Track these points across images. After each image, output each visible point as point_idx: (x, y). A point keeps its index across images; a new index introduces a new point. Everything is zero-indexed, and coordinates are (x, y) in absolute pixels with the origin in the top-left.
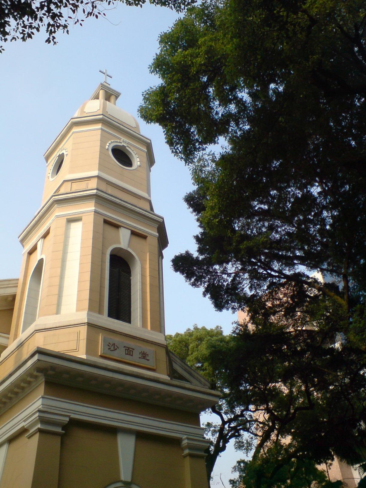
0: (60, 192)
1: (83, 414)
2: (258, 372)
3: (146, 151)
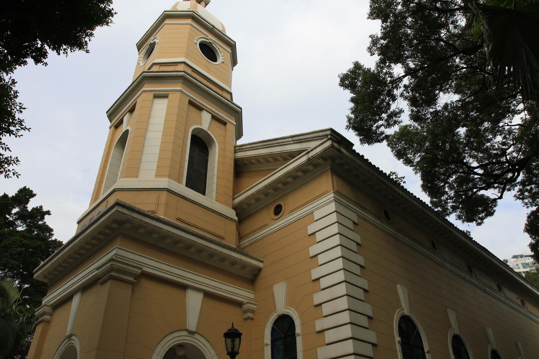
0: (152, 70)
3: (231, 52)
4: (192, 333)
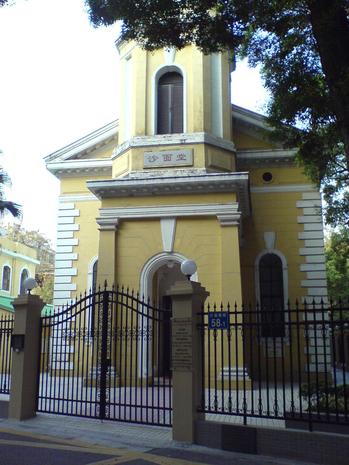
1: (130, 214)
2: (305, 135)
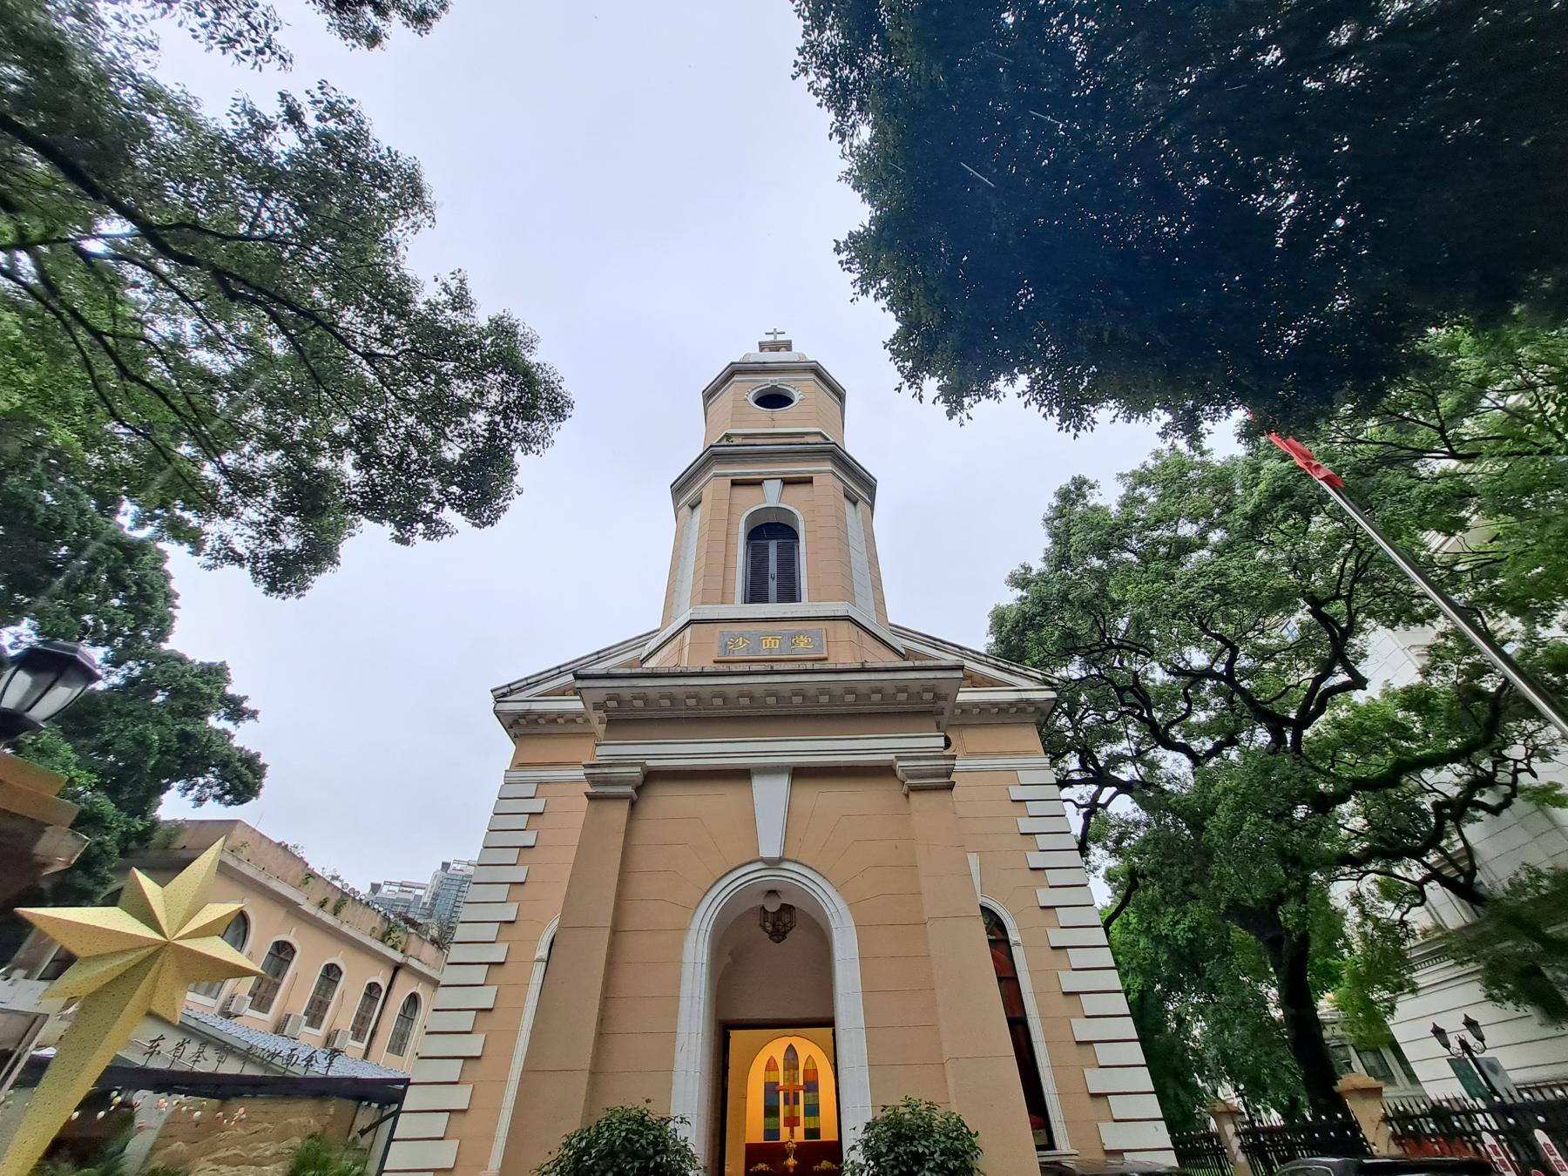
4: (773, 863)
